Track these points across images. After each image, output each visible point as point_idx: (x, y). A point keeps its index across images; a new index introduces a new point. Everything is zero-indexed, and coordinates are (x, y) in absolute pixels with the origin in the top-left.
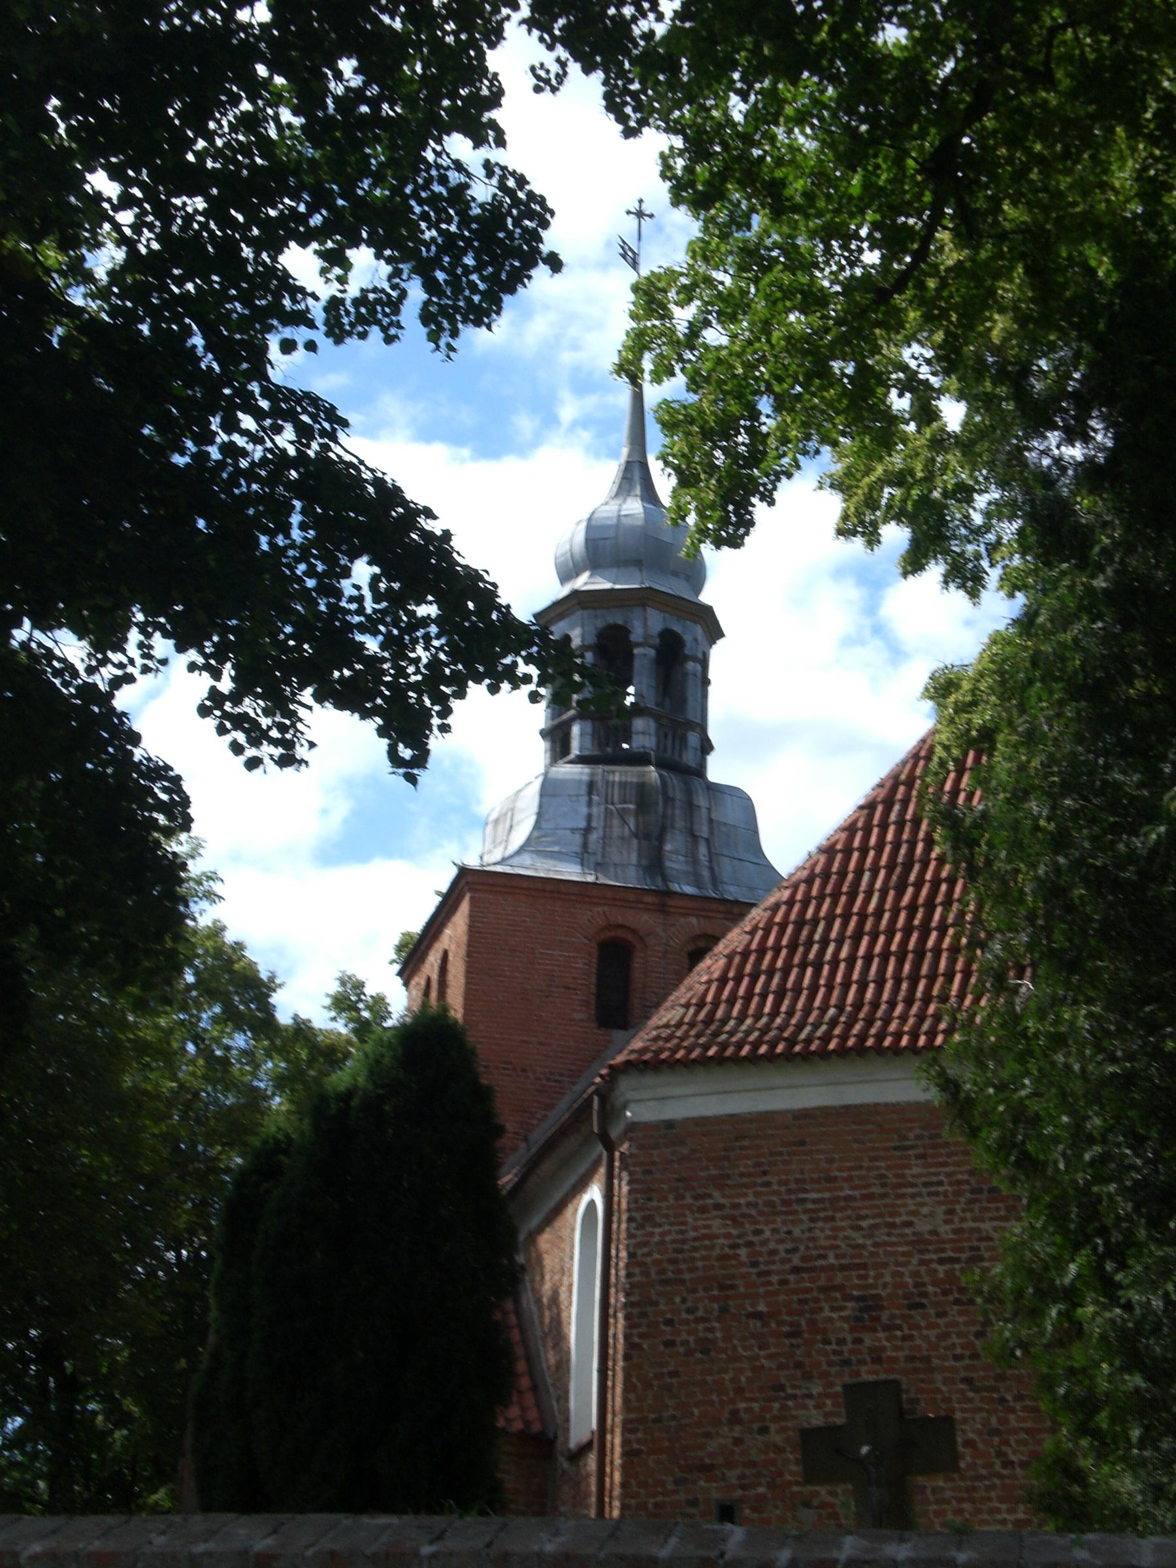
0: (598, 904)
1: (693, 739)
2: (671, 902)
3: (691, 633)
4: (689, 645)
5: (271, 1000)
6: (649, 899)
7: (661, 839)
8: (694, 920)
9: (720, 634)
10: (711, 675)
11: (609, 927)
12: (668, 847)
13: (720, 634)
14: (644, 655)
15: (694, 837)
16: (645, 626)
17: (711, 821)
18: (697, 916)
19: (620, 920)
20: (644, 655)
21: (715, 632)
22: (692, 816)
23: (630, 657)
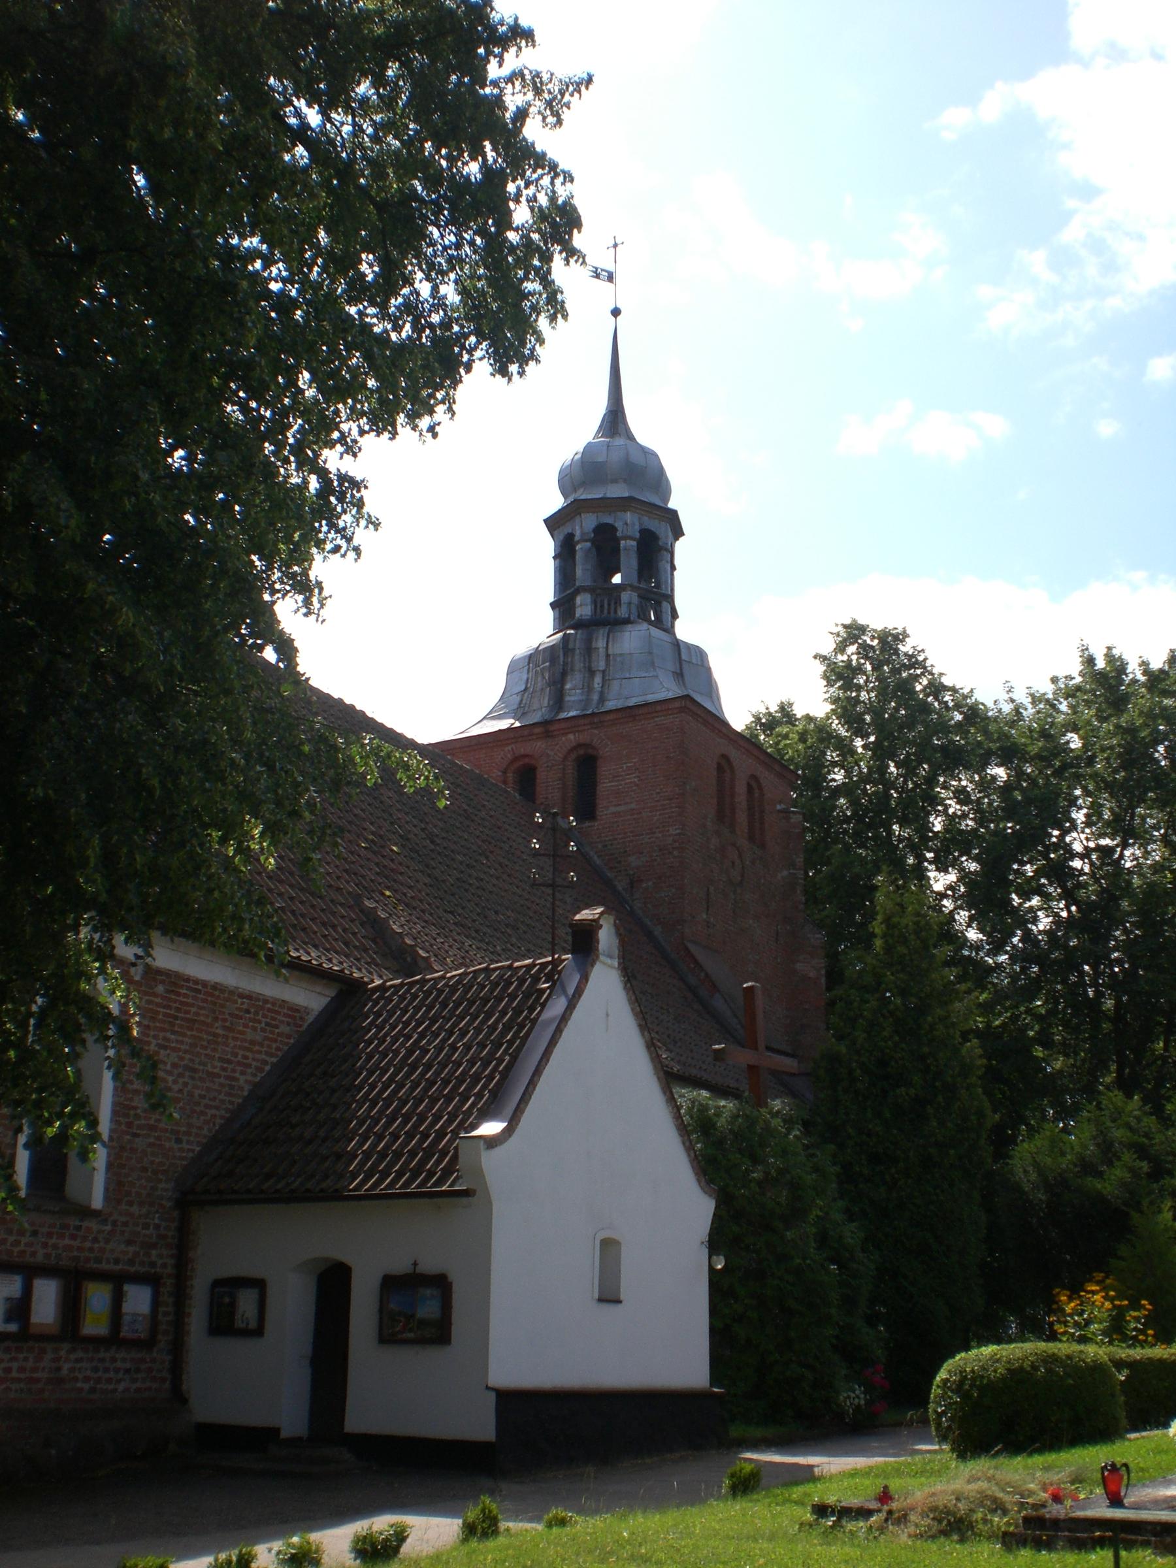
0: (508, 744)
1: (665, 605)
2: (552, 728)
3: (662, 530)
4: (620, 529)
5: (738, 718)
6: (537, 730)
7: (563, 682)
8: (571, 736)
9: (682, 534)
10: (676, 562)
11: (516, 759)
12: (568, 686)
13: (682, 534)
14: (629, 547)
15: (592, 673)
16: (628, 523)
17: (608, 656)
18: (574, 732)
19: (522, 751)
20: (629, 547)
21: (678, 532)
22: (590, 656)
23: (616, 550)
